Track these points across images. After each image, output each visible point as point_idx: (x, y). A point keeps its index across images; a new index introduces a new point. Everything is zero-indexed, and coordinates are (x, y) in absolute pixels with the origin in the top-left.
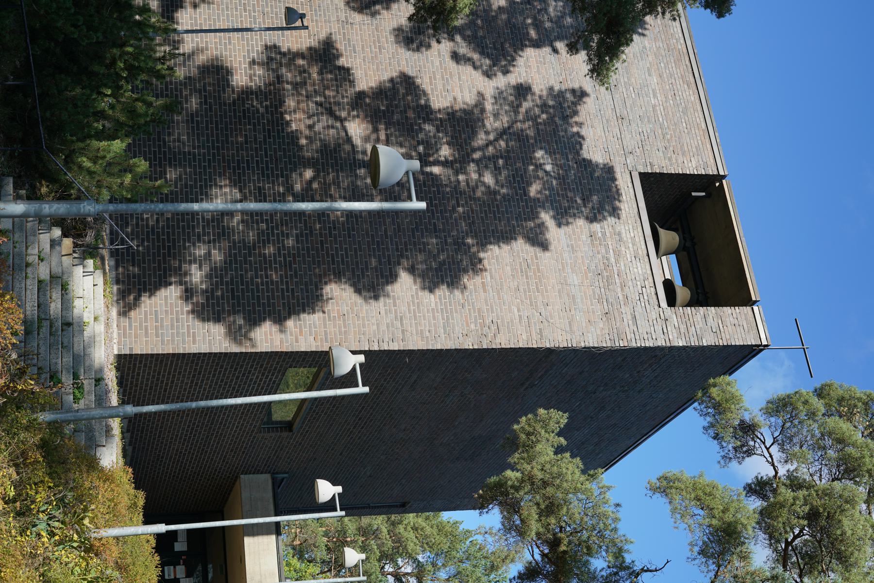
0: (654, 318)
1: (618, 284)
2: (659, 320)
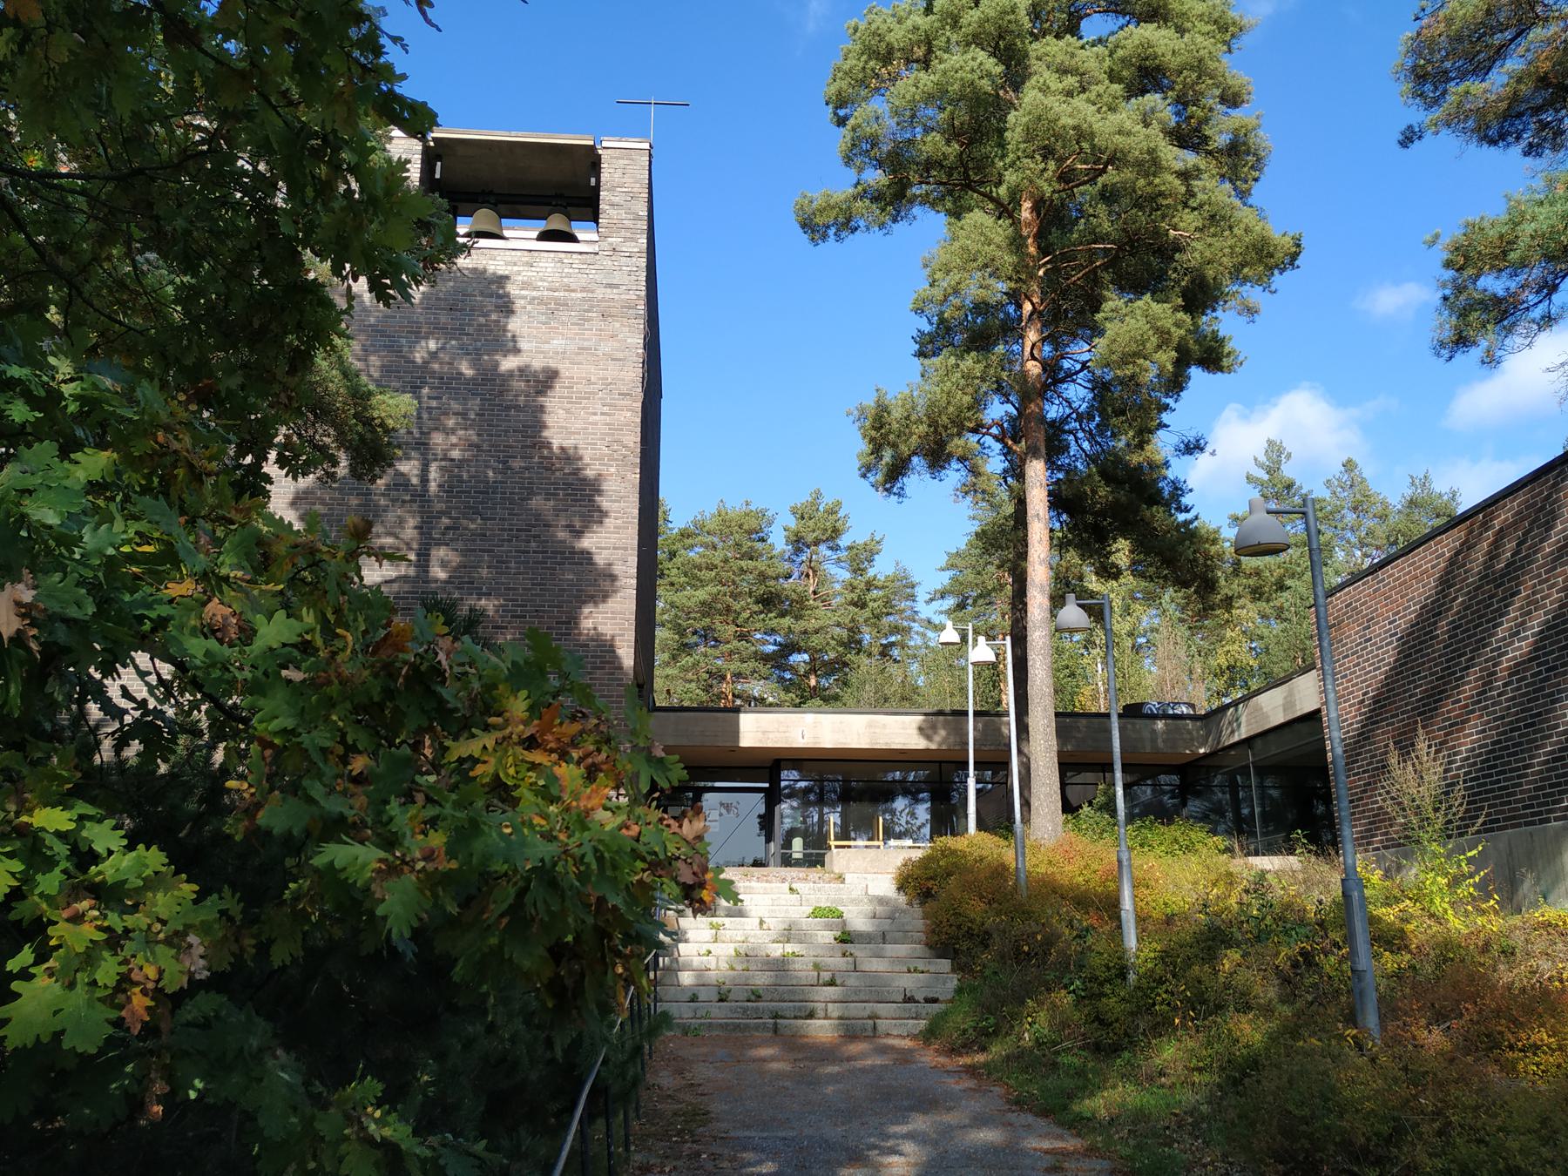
1: (566, 294)
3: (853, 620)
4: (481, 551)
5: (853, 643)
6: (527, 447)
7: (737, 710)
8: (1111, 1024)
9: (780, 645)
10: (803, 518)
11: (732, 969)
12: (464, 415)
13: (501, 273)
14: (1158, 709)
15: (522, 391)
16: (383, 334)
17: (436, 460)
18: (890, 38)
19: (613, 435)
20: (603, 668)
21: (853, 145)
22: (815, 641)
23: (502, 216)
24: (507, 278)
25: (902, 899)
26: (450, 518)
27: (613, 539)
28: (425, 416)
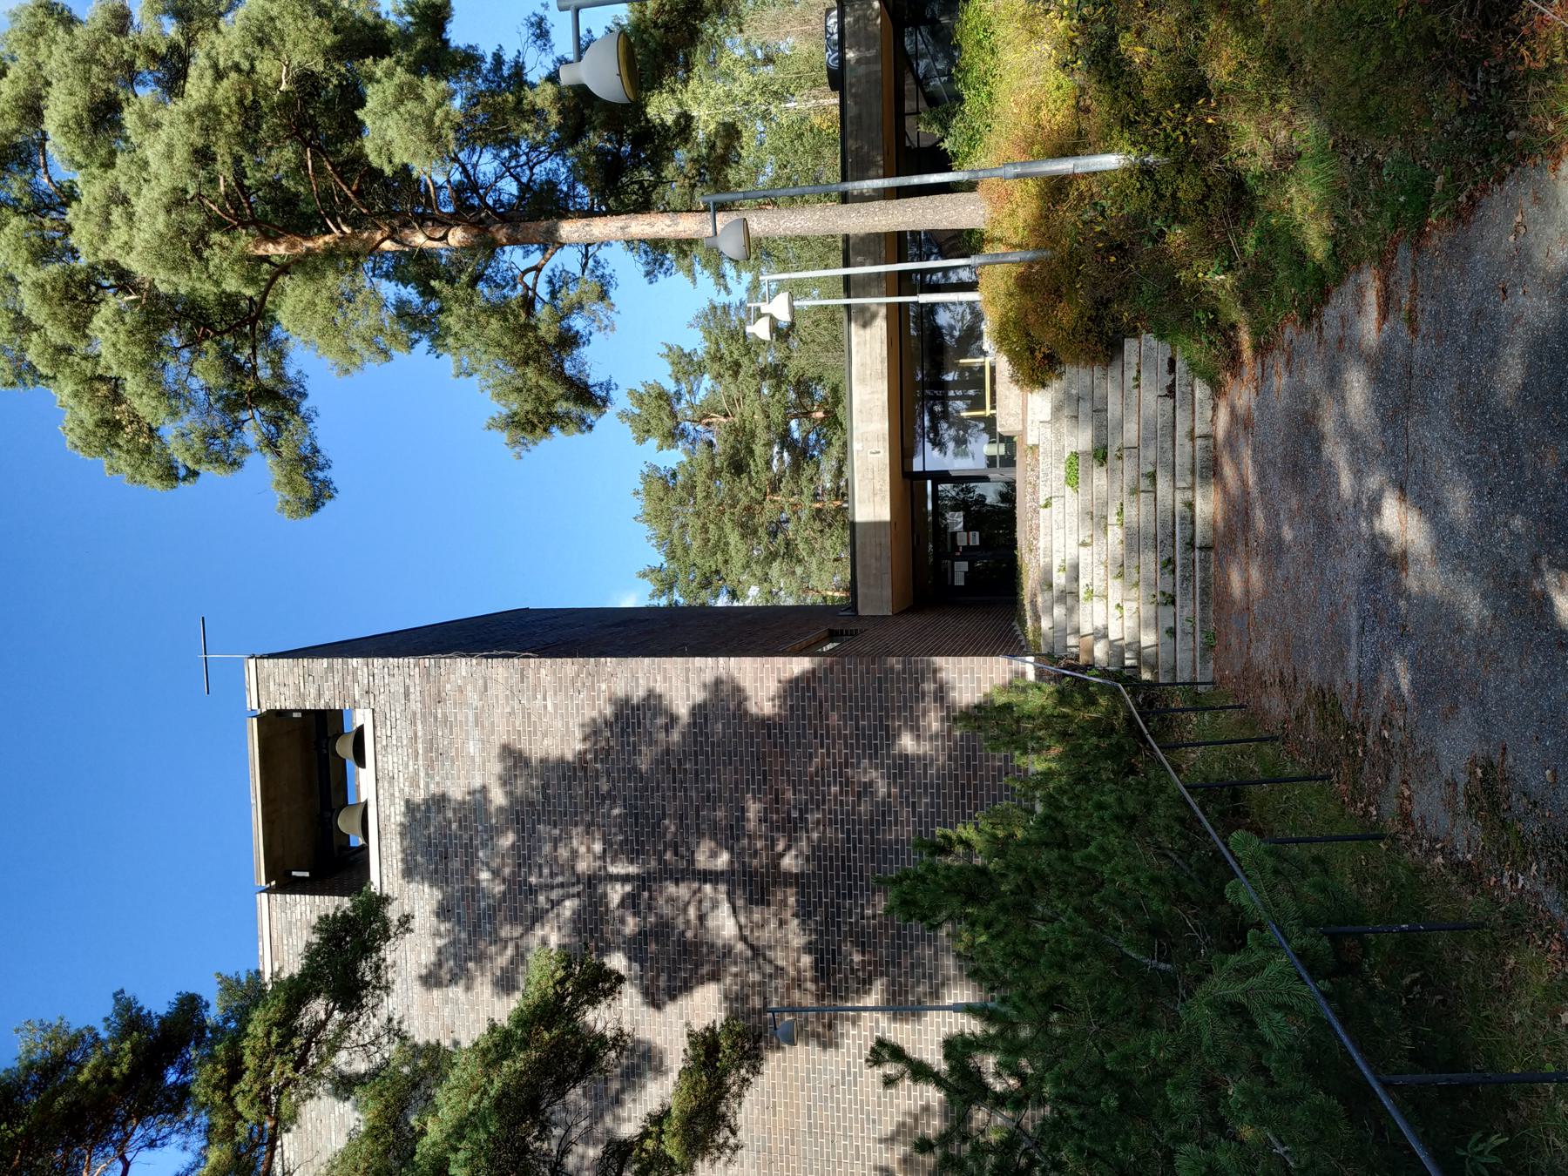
0: (382, 697)
1: (420, 741)
2: (377, 693)
3: (753, 376)
4: (698, 819)
5: (775, 373)
6: (586, 776)
7: (853, 525)
8: (1207, 186)
9: (782, 448)
10: (648, 431)
11: (1137, 584)
12: (556, 842)
13: (403, 809)
14: (833, 52)
15: (527, 782)
16: (477, 926)
17: (605, 867)
18: (90, 423)
19: (566, 687)
20: (814, 688)
21: (217, 461)
22: (776, 415)
23: (345, 804)
24: (407, 802)
25: (1056, 385)
26: (665, 851)
27: (677, 683)
28: (560, 879)
